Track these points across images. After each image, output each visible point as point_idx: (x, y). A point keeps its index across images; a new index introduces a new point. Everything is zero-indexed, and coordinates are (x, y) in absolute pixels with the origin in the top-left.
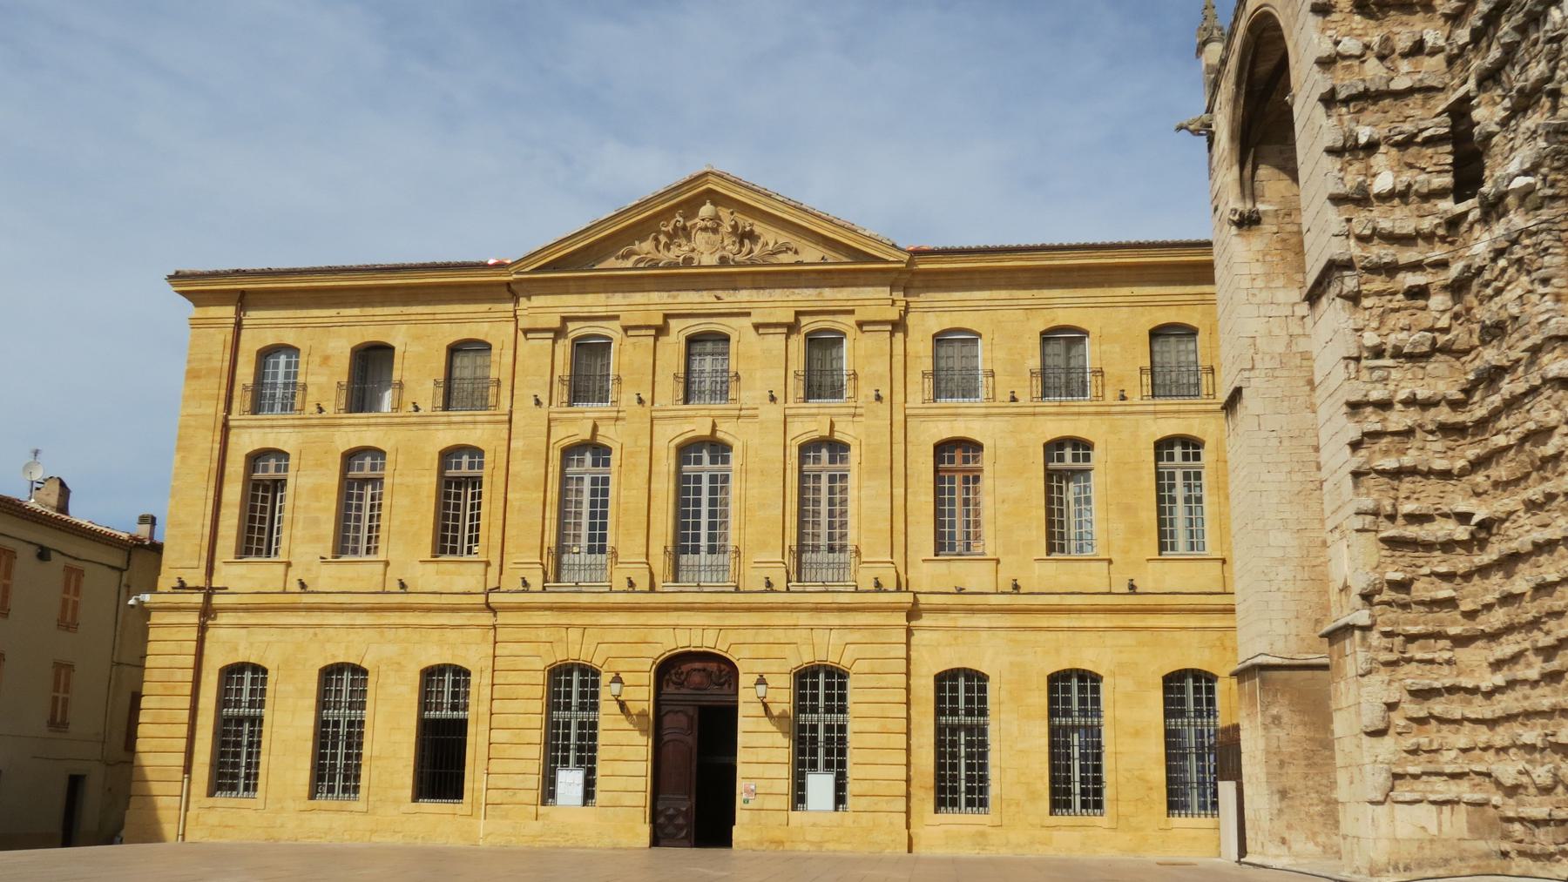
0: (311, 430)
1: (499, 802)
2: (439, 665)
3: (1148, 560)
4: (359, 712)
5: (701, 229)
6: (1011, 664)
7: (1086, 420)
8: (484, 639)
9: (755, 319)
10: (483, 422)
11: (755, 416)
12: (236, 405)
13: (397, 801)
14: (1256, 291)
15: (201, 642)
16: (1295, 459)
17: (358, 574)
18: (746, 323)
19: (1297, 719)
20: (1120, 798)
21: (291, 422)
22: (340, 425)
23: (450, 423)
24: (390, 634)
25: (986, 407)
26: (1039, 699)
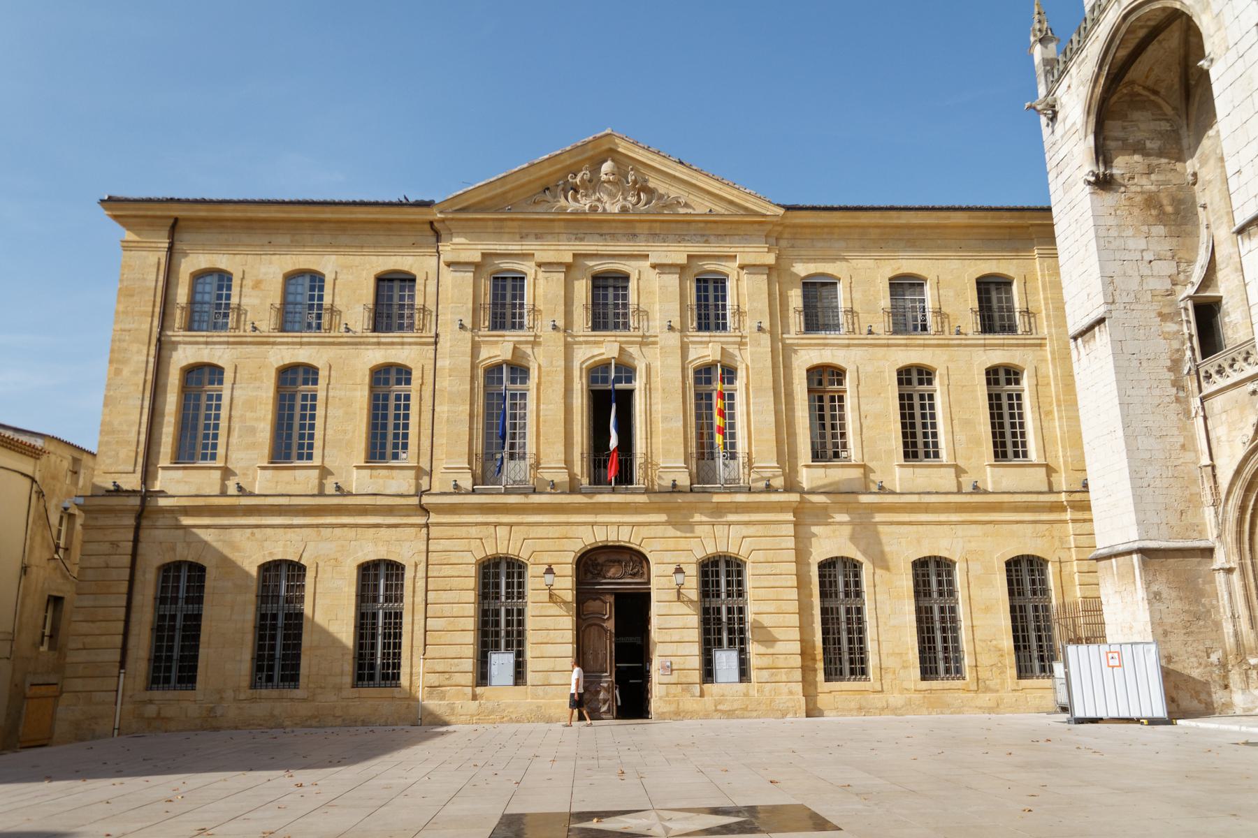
0: (245, 346)
1: (437, 684)
2: (374, 561)
4: (196, 606)
7: (929, 351)
9: (652, 260)
10: (410, 344)
14: (1111, 239)
16: (1153, 377)
18: (646, 264)
19: (1174, 594)
20: (978, 664)
23: (379, 344)
24: (326, 532)
25: (848, 339)
26: (470, 581)
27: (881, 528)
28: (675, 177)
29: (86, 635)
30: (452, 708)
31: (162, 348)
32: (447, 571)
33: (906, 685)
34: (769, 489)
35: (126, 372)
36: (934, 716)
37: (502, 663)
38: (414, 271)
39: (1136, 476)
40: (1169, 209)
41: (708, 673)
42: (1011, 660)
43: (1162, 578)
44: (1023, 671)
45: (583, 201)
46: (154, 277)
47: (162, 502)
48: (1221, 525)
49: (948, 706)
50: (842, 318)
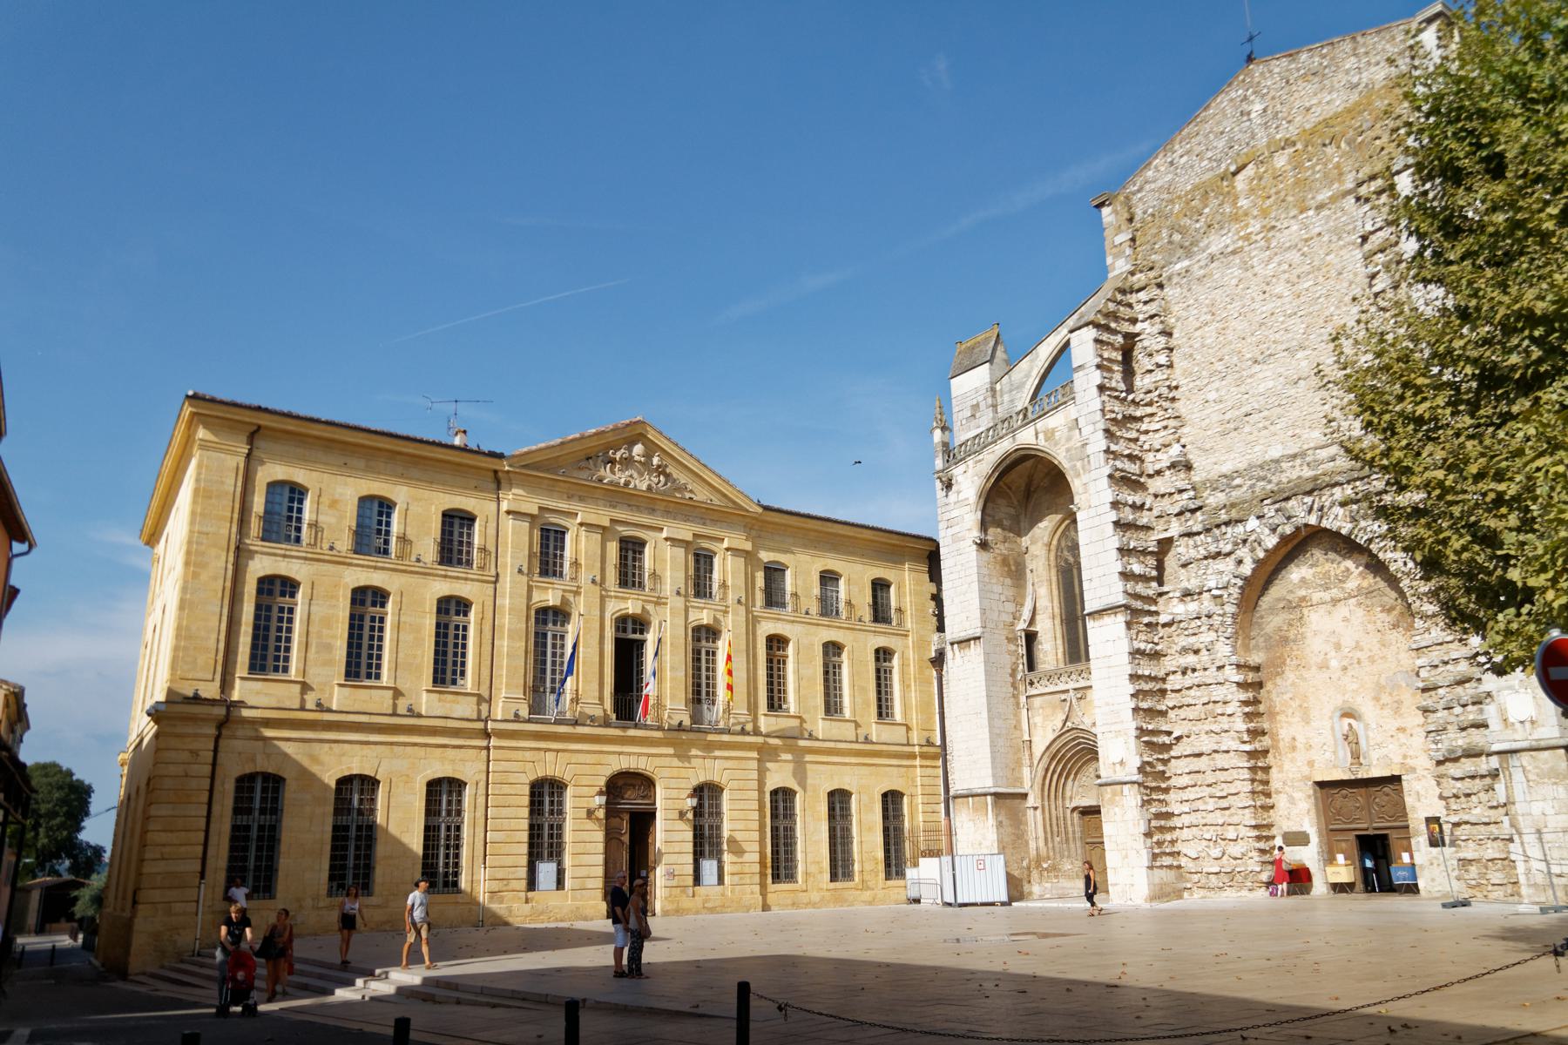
10: (473, 580)
17: (370, 700)
27: (808, 766)
28: (686, 467)
29: (164, 845)
30: (510, 910)
31: (241, 554)
32: (506, 789)
33: (821, 886)
34: (743, 732)
35: (204, 576)
36: (838, 908)
37: (546, 870)
38: (476, 513)
39: (993, 745)
40: (1013, 568)
42: (882, 867)
43: (1003, 812)
44: (888, 876)
45: (618, 474)
46: (233, 482)
47: (246, 713)
48: (1033, 780)
49: (846, 901)
50: (788, 598)
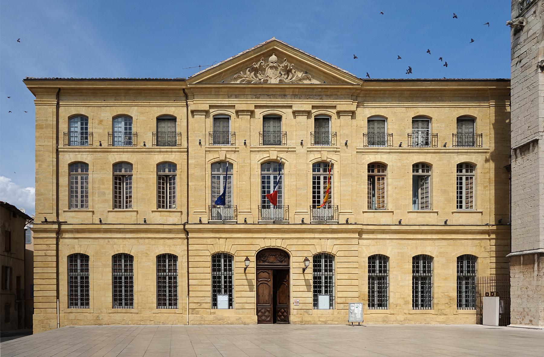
3: (408, 212)
5: (270, 67)
6: (398, 252)
8: (183, 244)
10: (175, 152)
11: (295, 151)
12: (61, 142)
13: (151, 309)
15: (57, 244)
18: (290, 111)
21: (88, 150)
22: (110, 152)
41: (215, 304)
